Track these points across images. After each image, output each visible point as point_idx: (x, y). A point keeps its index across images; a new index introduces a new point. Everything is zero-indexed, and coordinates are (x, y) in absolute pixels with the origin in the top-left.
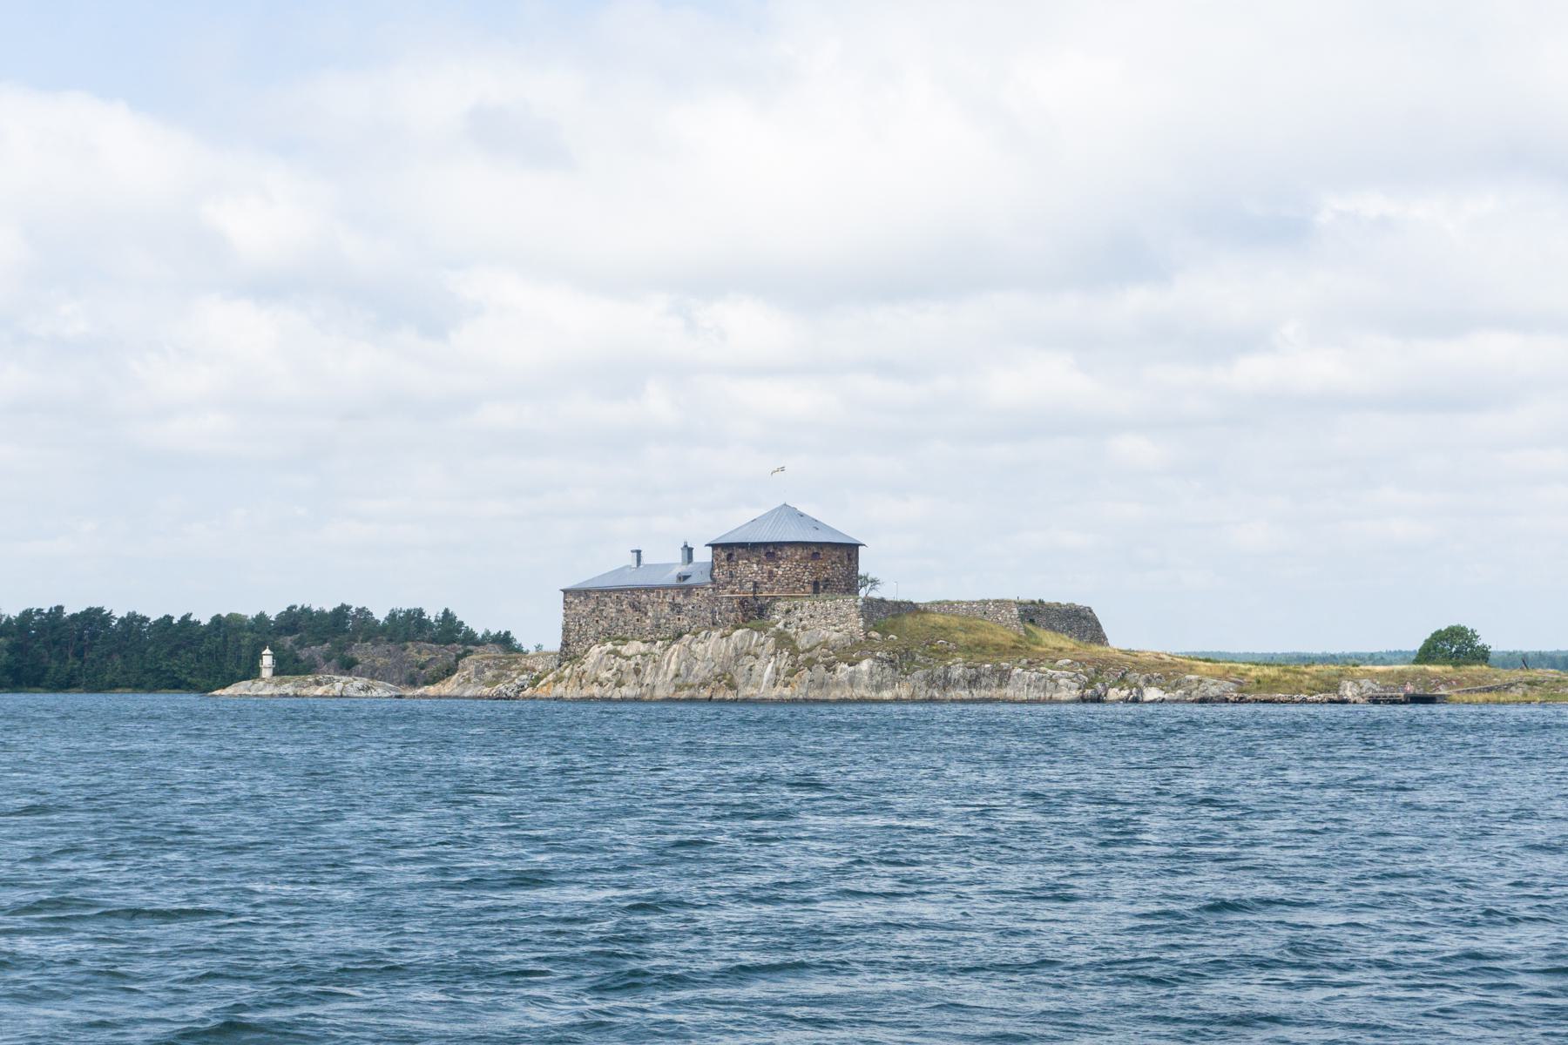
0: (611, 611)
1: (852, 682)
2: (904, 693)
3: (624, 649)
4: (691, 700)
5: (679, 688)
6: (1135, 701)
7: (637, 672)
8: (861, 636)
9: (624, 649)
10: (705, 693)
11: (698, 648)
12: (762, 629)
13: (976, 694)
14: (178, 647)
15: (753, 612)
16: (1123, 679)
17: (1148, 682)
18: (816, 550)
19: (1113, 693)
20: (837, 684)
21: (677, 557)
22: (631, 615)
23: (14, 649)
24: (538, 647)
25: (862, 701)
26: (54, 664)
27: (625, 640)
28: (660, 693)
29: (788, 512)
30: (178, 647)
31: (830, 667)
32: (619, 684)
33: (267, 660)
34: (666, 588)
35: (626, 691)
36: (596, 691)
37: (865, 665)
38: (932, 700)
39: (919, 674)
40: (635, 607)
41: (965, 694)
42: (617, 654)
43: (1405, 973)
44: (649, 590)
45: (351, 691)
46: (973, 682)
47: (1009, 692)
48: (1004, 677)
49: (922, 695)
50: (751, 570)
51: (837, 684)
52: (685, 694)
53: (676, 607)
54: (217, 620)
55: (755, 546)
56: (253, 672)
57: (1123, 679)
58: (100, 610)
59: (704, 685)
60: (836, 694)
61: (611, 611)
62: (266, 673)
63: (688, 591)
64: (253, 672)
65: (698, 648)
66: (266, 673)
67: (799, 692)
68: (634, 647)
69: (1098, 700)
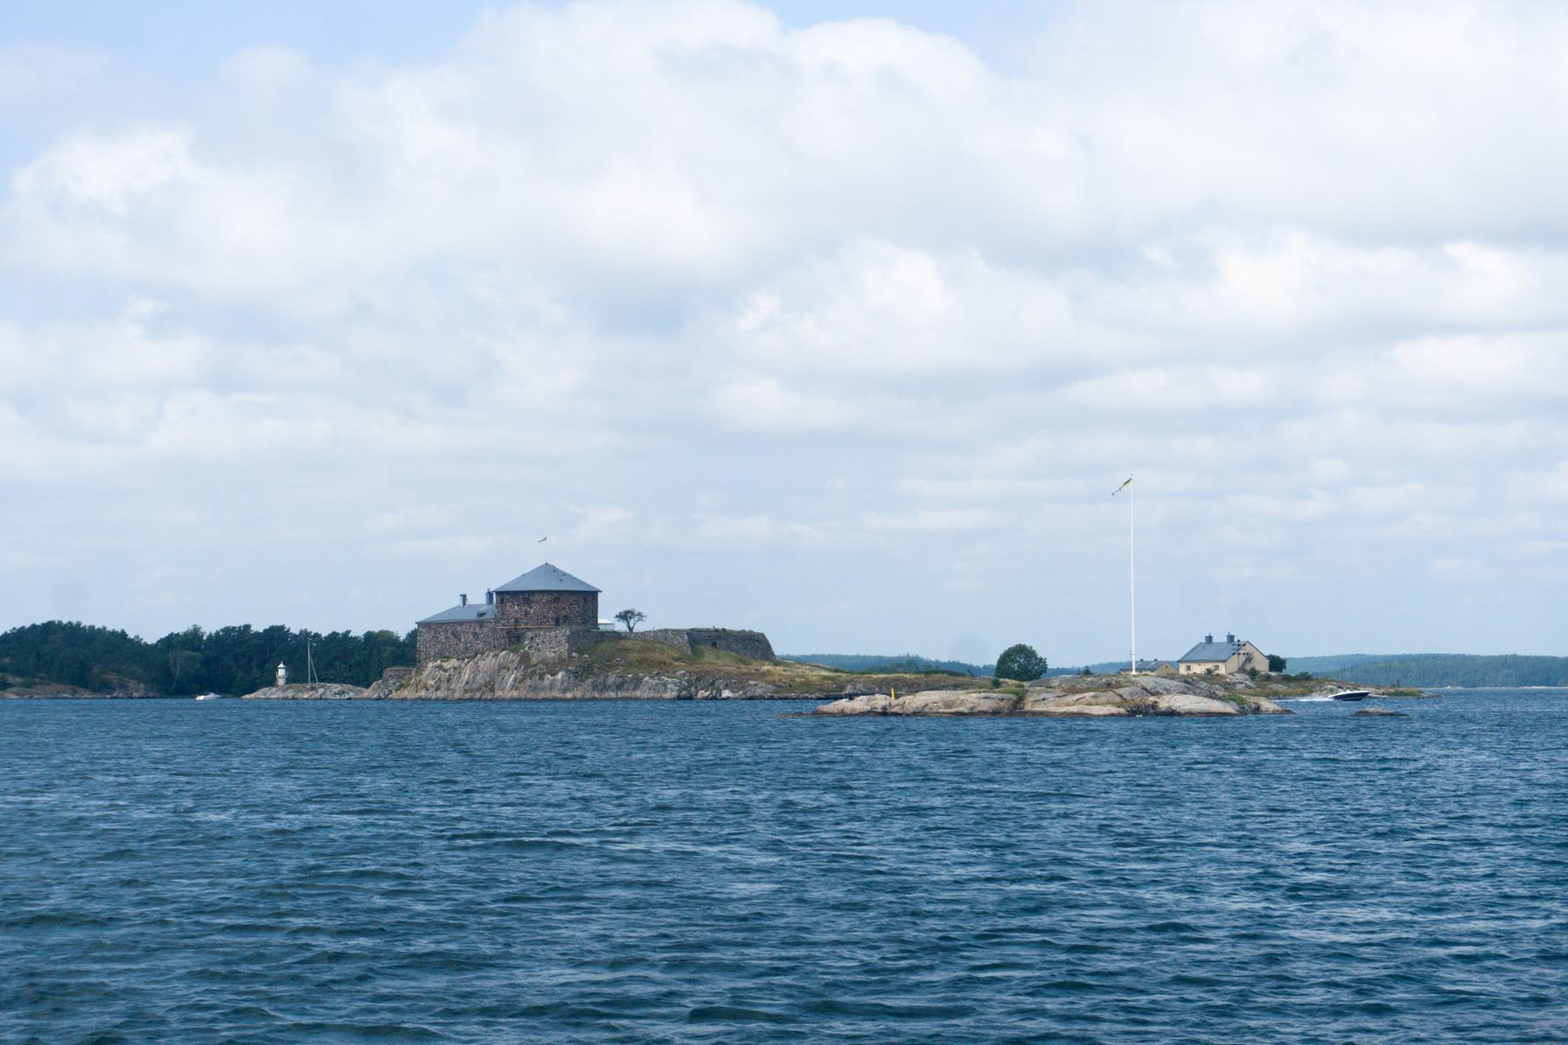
0: (442, 638)
1: (551, 687)
2: (579, 694)
3: (445, 665)
4: (471, 699)
5: (466, 691)
6: (714, 698)
7: (449, 680)
8: (565, 656)
9: (445, 665)
10: (478, 695)
11: (481, 663)
12: (515, 651)
13: (620, 694)
14: (336, 659)
15: (514, 638)
16: (712, 684)
17: (726, 686)
18: (557, 596)
19: (702, 694)
20: (544, 689)
21: (458, 602)
22: (453, 640)
23: (206, 662)
24: (1231, 638)
25: (555, 699)
26: (240, 673)
27: (449, 658)
28: (457, 695)
29: (549, 570)
30: (336, 659)
31: (542, 677)
32: (438, 689)
33: (281, 672)
34: (470, 622)
35: (440, 694)
36: (423, 693)
37: (559, 676)
38: (593, 699)
39: (589, 681)
40: (455, 635)
41: (613, 695)
42: (440, 667)
43: (1109, 936)
44: (461, 623)
45: (329, 695)
46: (619, 687)
47: (638, 693)
48: (637, 682)
49: (588, 695)
50: (514, 609)
51: (544, 689)
52: (468, 695)
53: (475, 635)
54: (369, 635)
55: (516, 593)
56: (272, 682)
57: (712, 684)
58: (282, 628)
59: (479, 689)
60: (542, 695)
61: (442, 638)
62: (281, 682)
63: (481, 624)
64: (272, 682)
65: (481, 663)
66: (281, 682)
67: (523, 693)
68: (454, 662)
69: (690, 698)
